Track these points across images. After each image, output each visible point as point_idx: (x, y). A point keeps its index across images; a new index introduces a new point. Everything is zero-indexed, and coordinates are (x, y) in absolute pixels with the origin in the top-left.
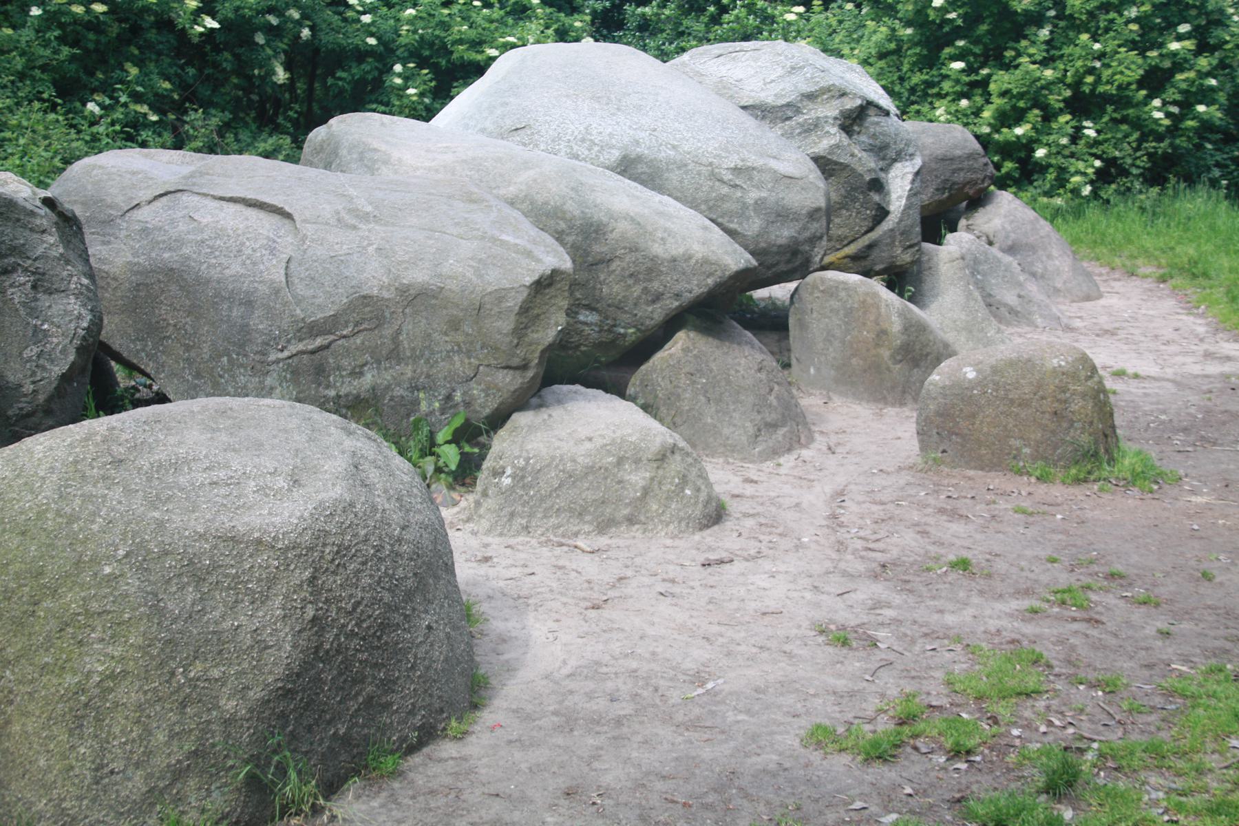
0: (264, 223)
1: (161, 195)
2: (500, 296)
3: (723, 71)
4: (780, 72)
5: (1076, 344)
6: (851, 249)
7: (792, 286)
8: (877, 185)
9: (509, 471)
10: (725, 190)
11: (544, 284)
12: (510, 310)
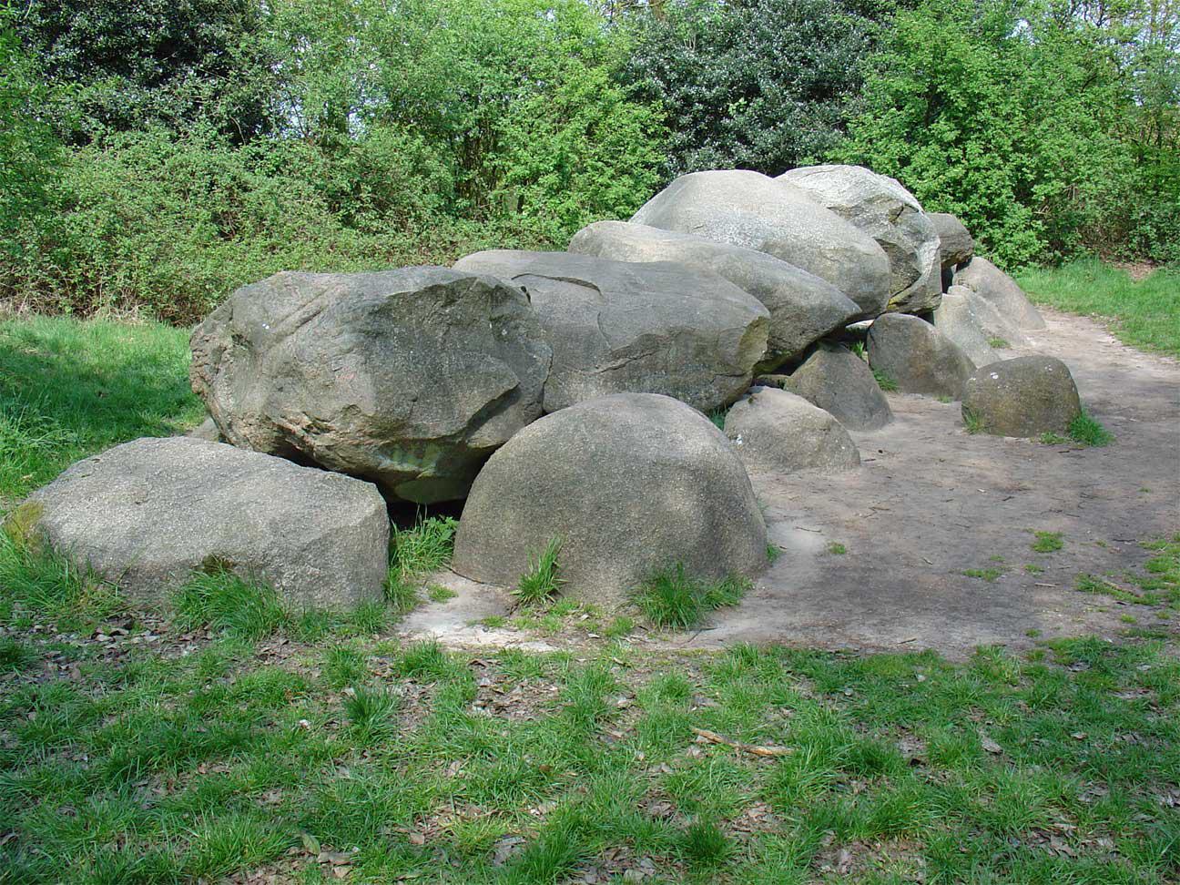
0: (585, 295)
1: (586, 284)
2: (730, 333)
3: (811, 185)
4: (848, 185)
5: (1005, 355)
6: (898, 298)
7: (870, 322)
8: (913, 256)
9: (740, 436)
10: (829, 263)
11: (756, 325)
12: (735, 341)
